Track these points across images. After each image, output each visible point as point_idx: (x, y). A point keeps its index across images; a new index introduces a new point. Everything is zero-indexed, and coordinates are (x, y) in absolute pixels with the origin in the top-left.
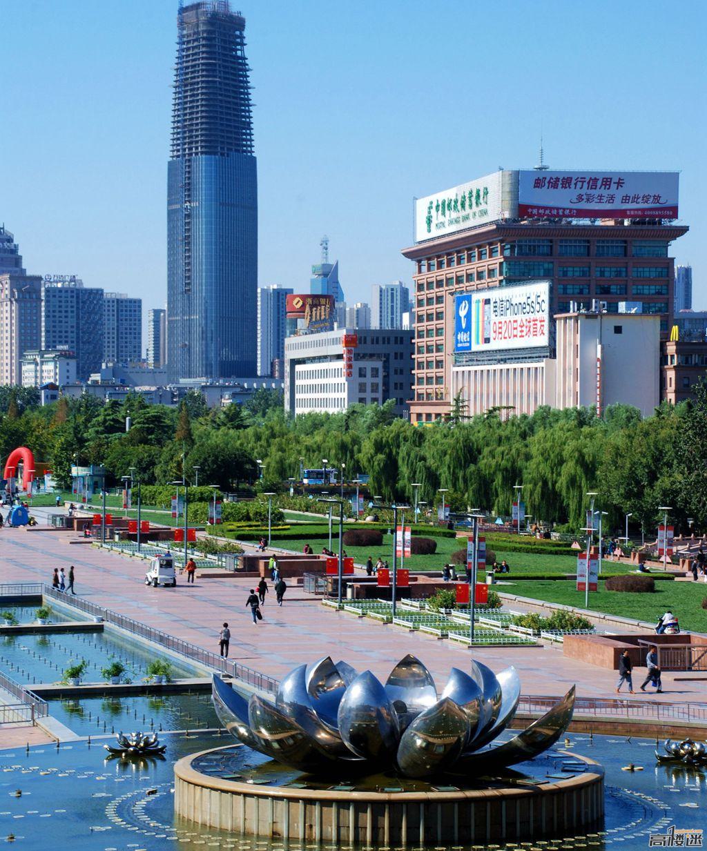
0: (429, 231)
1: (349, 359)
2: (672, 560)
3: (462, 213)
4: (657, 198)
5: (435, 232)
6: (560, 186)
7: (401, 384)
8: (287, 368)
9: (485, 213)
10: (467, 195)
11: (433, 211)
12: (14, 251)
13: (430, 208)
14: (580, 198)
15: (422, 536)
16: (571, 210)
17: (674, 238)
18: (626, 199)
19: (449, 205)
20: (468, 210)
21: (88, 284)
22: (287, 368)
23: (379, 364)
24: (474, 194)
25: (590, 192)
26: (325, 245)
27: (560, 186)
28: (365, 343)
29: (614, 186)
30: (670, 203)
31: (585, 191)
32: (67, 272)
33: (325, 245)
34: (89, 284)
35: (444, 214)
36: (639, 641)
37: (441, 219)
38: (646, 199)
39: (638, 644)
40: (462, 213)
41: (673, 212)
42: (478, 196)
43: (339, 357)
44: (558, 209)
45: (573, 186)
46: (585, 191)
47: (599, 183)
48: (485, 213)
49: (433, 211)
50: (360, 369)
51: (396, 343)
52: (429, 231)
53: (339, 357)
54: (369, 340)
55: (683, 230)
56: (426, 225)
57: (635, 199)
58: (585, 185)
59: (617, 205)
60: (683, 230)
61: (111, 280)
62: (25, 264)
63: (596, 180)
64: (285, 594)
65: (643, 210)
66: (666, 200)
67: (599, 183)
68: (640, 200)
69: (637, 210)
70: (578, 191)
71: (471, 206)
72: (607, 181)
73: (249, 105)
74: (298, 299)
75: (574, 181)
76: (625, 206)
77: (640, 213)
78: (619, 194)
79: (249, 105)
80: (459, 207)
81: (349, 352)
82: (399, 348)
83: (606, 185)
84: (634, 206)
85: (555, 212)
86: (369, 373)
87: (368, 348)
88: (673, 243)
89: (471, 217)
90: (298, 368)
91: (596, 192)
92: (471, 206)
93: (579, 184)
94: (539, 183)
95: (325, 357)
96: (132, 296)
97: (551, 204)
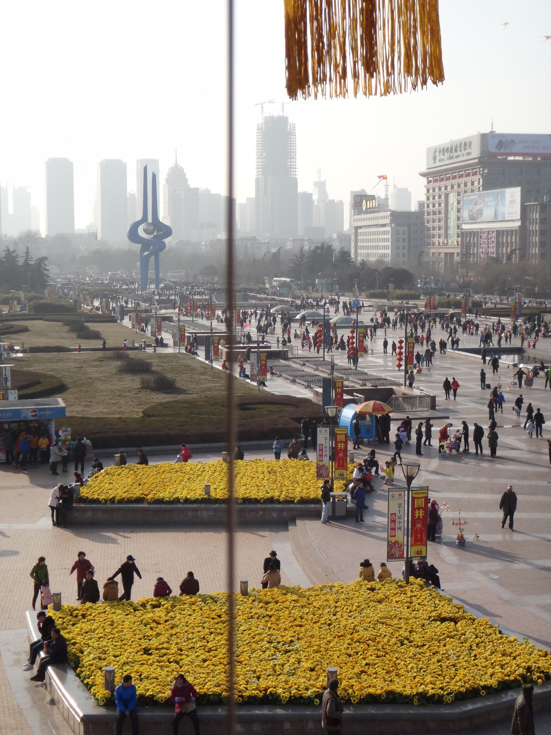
0: (435, 162)
3: (455, 154)
5: (438, 164)
9: (469, 154)
11: (437, 154)
12: (4, 556)
15: (410, 527)
19: (447, 150)
20: (459, 153)
23: (406, 228)
24: (463, 144)
26: (319, 172)
33: (319, 172)
35: (444, 154)
36: (355, 394)
39: (353, 396)
40: (455, 154)
49: (437, 154)
62: (189, 183)
64: (298, 493)
73: (295, 168)
79: (295, 168)
80: (454, 151)
89: (461, 156)
90: (359, 231)
92: (461, 151)
95: (370, 226)
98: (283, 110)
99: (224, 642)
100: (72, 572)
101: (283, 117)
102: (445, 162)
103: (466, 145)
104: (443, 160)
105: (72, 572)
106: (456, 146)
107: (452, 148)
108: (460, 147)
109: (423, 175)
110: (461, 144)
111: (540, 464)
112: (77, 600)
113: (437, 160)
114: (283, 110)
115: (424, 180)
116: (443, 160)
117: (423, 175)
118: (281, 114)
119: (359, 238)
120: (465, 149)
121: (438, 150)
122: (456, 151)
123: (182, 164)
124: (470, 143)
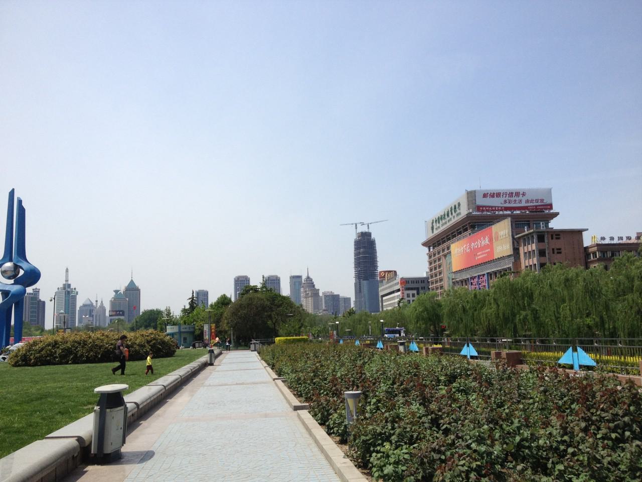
0: (433, 232)
1: (403, 290)
2: (478, 352)
4: (542, 200)
5: (436, 232)
6: (495, 196)
7: (424, 287)
8: (380, 299)
9: (459, 214)
10: (450, 210)
12: (313, 283)
13: (433, 223)
14: (505, 202)
16: (501, 207)
17: (552, 218)
18: (527, 201)
19: (441, 218)
21: (335, 293)
22: (380, 299)
23: (415, 292)
25: (509, 199)
27: (495, 196)
28: (409, 283)
29: (521, 196)
30: (548, 202)
31: (507, 198)
32: (330, 290)
34: (336, 293)
35: (439, 222)
37: (438, 225)
38: (537, 201)
41: (550, 206)
42: (455, 208)
43: (399, 290)
44: (495, 207)
45: (501, 196)
46: (507, 198)
47: (514, 195)
48: (459, 214)
49: (434, 224)
50: (407, 294)
51: (421, 282)
52: (433, 232)
53: (399, 290)
54: (410, 282)
55: (556, 214)
56: (431, 231)
57: (532, 201)
58: (508, 196)
59: (523, 204)
60: (556, 214)
61: (343, 294)
63: (512, 193)
65: (536, 206)
66: (546, 201)
67: (514, 195)
68: (534, 202)
69: (533, 206)
70: (504, 199)
71: (452, 214)
72: (517, 194)
74: (383, 273)
75: (502, 194)
76: (527, 205)
77: (535, 207)
78: (524, 199)
81: (402, 287)
82: (423, 285)
83: (517, 195)
84: (532, 204)
85: (494, 208)
86: (411, 296)
87: (411, 286)
88: (552, 221)
90: (384, 298)
91: (513, 199)
92: (452, 214)
93: (504, 195)
94: (485, 196)
96: (348, 297)
97: (492, 205)
98: (368, 228)
99: (265, 347)
100: (146, 456)
101: (368, 232)
102: (441, 228)
103: (455, 208)
104: (439, 227)
105: (146, 456)
106: (448, 212)
107: (444, 215)
108: (451, 211)
109: (424, 244)
110: (451, 208)
111: (283, 397)
112: (133, 291)
113: (435, 230)
114: (368, 228)
115: (426, 249)
116: (439, 227)
117: (424, 244)
118: (367, 231)
119: (384, 304)
120: (455, 211)
121: (435, 220)
122: (448, 215)
123: (311, 276)
124: (459, 204)
